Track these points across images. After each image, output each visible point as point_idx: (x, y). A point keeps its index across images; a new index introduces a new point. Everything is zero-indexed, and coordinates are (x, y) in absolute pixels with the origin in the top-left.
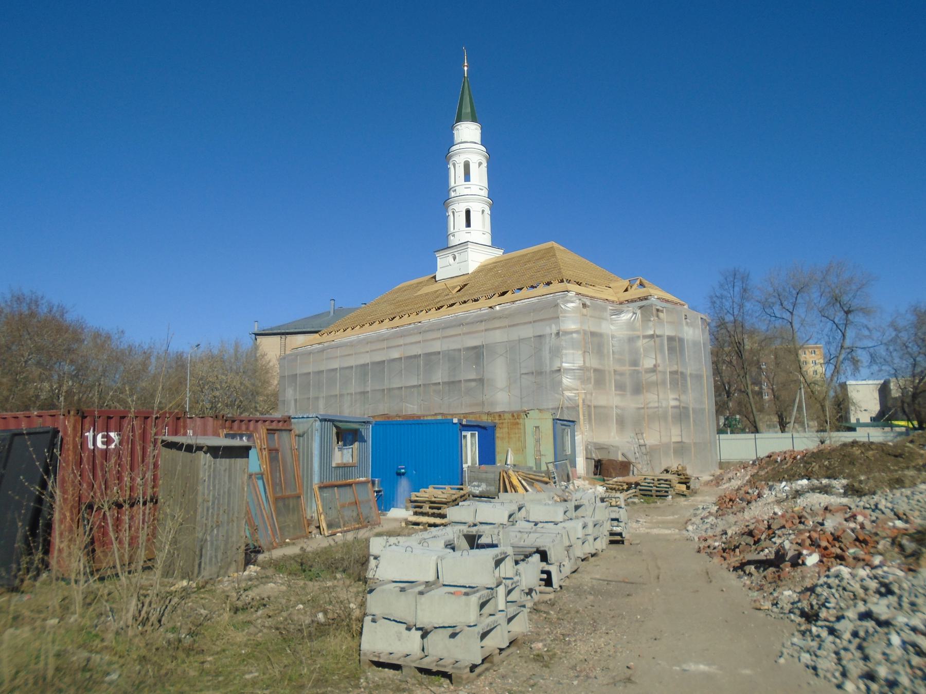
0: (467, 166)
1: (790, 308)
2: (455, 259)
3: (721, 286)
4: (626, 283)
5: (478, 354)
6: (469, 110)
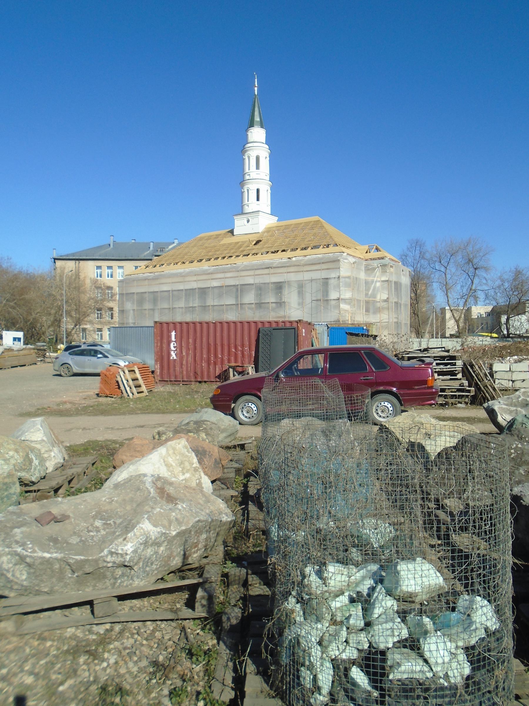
0: (258, 158)
2: (248, 221)
4: (366, 247)
5: (279, 287)
6: (258, 119)
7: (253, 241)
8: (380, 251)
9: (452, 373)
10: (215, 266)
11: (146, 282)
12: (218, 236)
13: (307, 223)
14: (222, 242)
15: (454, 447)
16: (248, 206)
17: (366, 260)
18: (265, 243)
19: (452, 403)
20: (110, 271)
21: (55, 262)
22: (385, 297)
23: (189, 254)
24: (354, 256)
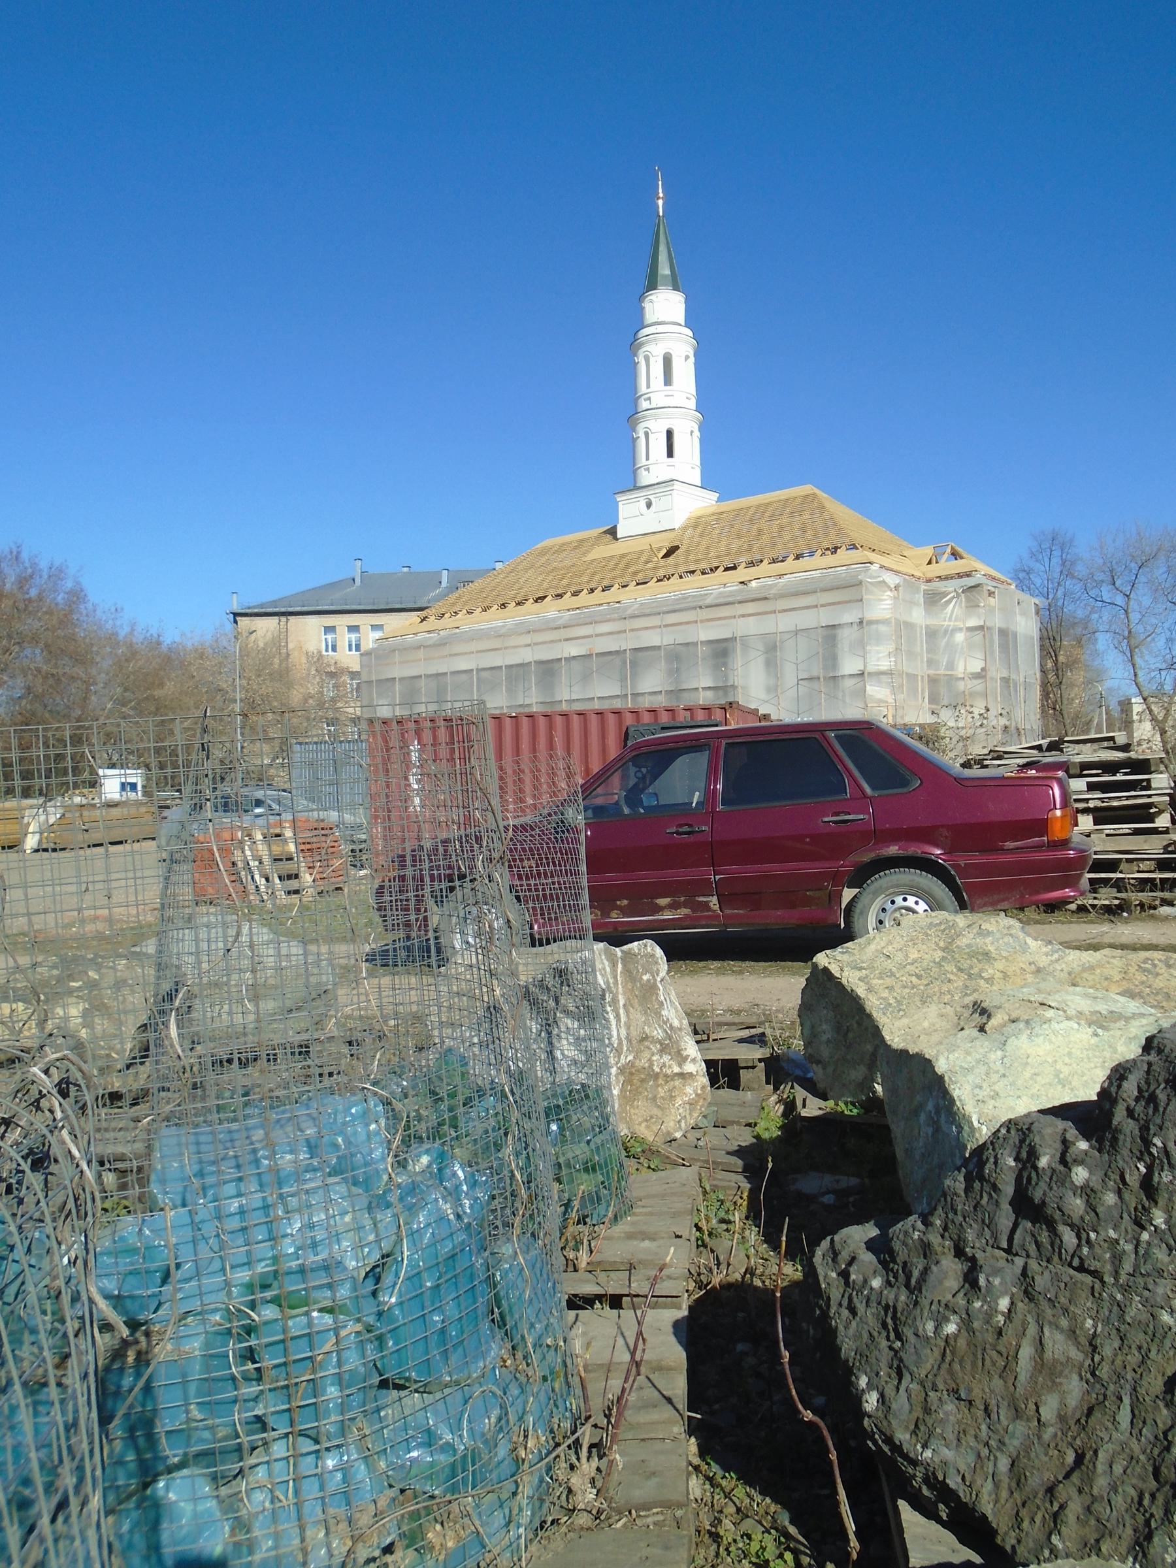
0: (667, 361)
1: (1127, 589)
2: (649, 505)
3: (1033, 555)
4: (928, 551)
6: (667, 272)
7: (659, 550)
8: (962, 558)
9: (1143, 813)
10: (573, 609)
11: (421, 654)
12: (581, 543)
13: (789, 501)
14: (592, 555)
15: (1091, 1118)
16: (648, 470)
17: (929, 581)
18: (688, 552)
19: (1142, 905)
20: (353, 636)
21: (236, 622)
22: (976, 666)
23: (515, 587)
24: (896, 572)
